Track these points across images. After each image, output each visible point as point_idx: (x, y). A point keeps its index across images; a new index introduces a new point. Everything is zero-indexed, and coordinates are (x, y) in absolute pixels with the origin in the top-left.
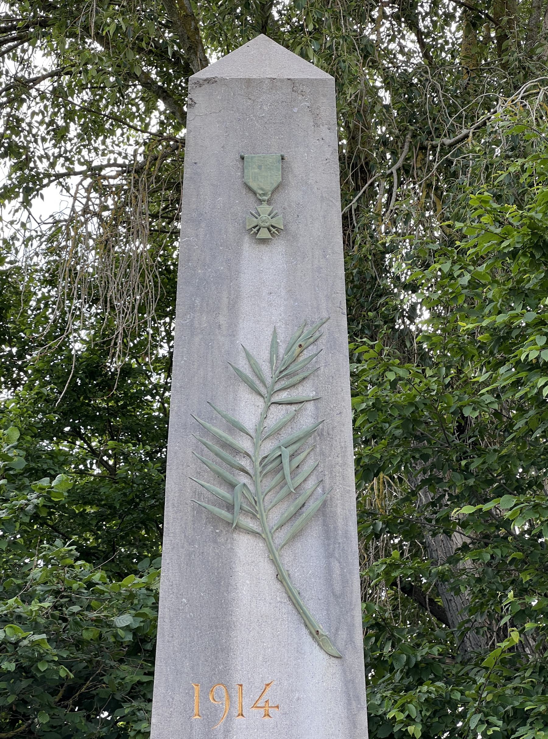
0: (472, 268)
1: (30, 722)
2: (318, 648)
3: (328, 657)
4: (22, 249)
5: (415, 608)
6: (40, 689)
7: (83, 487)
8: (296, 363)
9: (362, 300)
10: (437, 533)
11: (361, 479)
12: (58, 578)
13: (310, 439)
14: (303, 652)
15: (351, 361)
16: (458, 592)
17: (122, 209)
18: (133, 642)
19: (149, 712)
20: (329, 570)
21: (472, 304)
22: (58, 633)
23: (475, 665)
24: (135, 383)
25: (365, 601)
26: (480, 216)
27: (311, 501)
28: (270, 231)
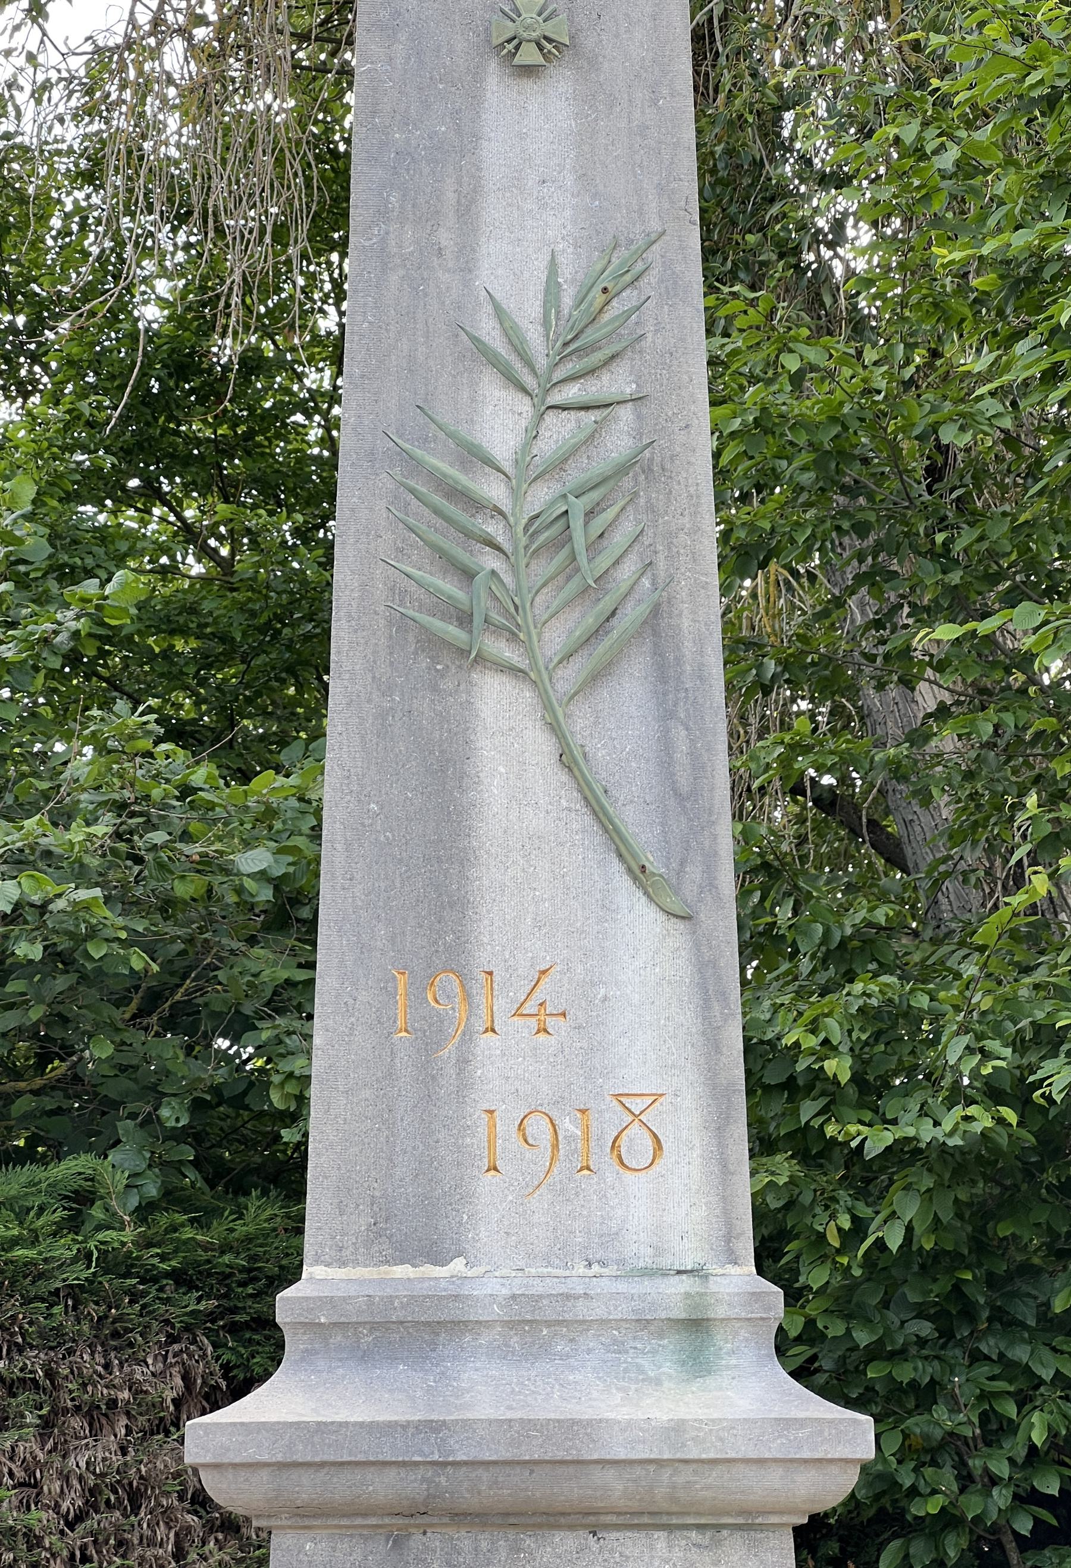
0: (963, 134)
1: (74, 1058)
2: (644, 899)
3: (665, 917)
4: (29, 110)
5: (841, 840)
6: (94, 993)
7: (167, 602)
8: (596, 325)
9: (733, 209)
10: (886, 683)
11: (733, 573)
12: (121, 777)
13: (625, 479)
14: (614, 907)
15: (709, 333)
16: (926, 799)
17: (235, 19)
18: (275, 904)
19: (308, 1037)
20: (666, 745)
21: (963, 213)
22: (125, 886)
23: (958, 943)
24: (271, 388)
25: (741, 819)
26: (981, 25)
27: (630, 605)
28: (541, 48)
